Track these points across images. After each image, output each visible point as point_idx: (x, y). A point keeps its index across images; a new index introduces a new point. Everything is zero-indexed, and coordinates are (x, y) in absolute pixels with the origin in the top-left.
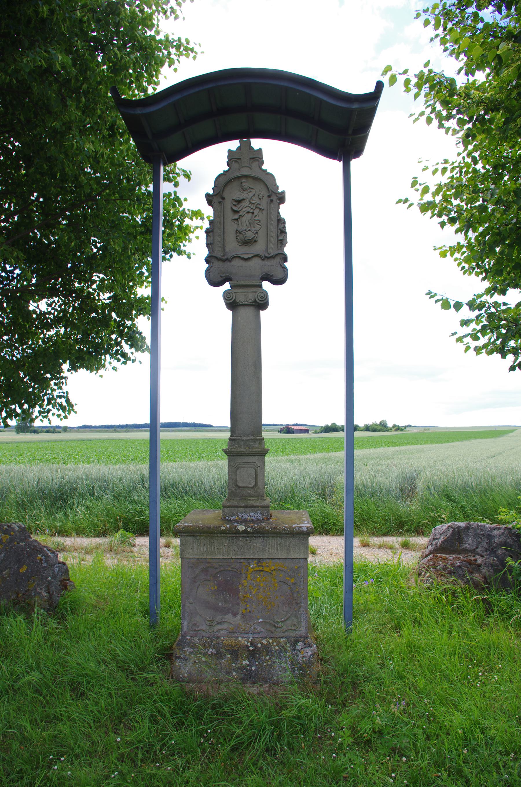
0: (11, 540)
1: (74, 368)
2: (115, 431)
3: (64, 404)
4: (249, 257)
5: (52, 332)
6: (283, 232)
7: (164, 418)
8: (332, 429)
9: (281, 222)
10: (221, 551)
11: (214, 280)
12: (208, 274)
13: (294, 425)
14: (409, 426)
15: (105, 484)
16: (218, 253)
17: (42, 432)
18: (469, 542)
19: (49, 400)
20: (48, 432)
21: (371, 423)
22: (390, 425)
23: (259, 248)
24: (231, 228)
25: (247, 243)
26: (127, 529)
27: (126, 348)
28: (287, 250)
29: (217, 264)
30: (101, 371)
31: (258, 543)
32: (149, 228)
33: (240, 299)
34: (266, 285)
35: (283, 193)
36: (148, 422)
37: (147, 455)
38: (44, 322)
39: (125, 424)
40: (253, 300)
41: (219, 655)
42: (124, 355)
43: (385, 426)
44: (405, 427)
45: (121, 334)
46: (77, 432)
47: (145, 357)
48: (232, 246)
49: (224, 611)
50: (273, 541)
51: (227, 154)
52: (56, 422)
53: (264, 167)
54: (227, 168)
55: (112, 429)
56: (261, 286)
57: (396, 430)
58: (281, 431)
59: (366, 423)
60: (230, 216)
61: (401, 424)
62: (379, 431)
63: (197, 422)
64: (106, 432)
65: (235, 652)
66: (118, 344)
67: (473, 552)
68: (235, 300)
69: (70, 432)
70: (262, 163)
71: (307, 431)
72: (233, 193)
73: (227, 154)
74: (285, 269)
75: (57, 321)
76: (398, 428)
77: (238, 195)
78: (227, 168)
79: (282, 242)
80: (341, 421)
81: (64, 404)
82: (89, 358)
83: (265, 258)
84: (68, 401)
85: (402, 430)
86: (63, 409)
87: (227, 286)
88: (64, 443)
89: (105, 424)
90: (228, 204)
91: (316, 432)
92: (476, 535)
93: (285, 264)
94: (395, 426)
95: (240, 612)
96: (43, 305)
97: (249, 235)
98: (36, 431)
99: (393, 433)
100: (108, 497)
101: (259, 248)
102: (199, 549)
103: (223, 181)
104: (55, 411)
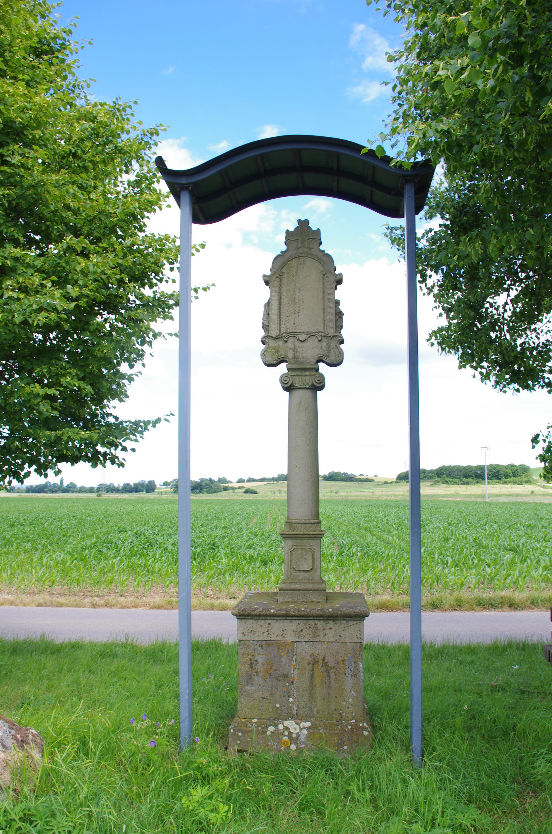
6: (339, 315)
8: (435, 606)
12: (264, 354)
28: (344, 333)
33: (297, 382)
34: (323, 368)
35: (341, 275)
38: (248, 569)
40: (310, 384)
51: (284, 235)
53: (322, 248)
54: (284, 248)
56: (317, 370)
68: (292, 384)
70: (321, 243)
73: (285, 235)
74: (341, 353)
78: (284, 248)
79: (339, 327)
87: (283, 368)
93: (341, 346)
95: (59, 433)
103: (281, 260)
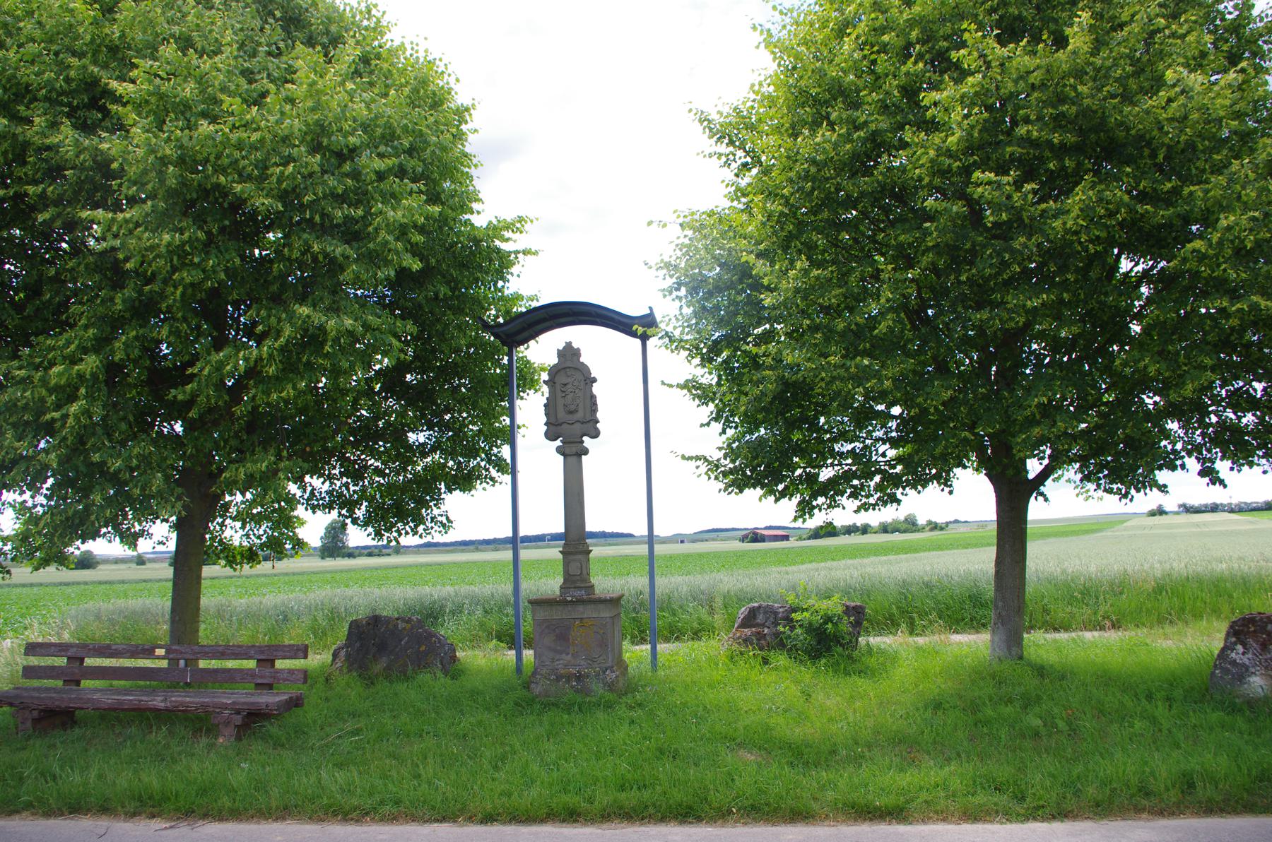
0: (412, 628)
1: (450, 490)
2: (477, 550)
3: (445, 521)
4: (573, 422)
5: (429, 459)
7: (522, 533)
9: (593, 397)
10: (558, 614)
11: (550, 436)
13: (766, 528)
14: (956, 521)
15: (476, 601)
16: (553, 421)
17: (360, 555)
18: (760, 618)
19: (432, 519)
20: (370, 555)
21: (890, 520)
22: (921, 521)
23: (579, 416)
24: (560, 402)
25: (571, 412)
26: (500, 639)
27: (493, 472)
28: (599, 415)
29: (553, 428)
30: (473, 492)
31: (581, 608)
32: (506, 380)
33: (567, 451)
36: (561, 529)
37: (521, 568)
38: (423, 451)
39: (491, 537)
41: (558, 679)
42: (492, 479)
43: (914, 524)
44: (947, 524)
45: (489, 461)
46: (416, 553)
47: (507, 478)
48: (562, 415)
49: (560, 653)
50: (590, 607)
52: (438, 538)
55: (471, 547)
57: (932, 530)
58: (743, 539)
59: (883, 520)
60: (559, 394)
61: (940, 519)
62: (905, 531)
63: (608, 529)
64: (463, 551)
65: (569, 678)
66: (487, 470)
67: (763, 625)
69: (405, 553)
71: (786, 538)
72: (561, 379)
75: (434, 449)
76: (934, 526)
77: (564, 380)
80: (641, 530)
81: (445, 521)
82: (464, 481)
83: (583, 423)
84: (448, 518)
85: (942, 529)
86: (444, 525)
88: (400, 570)
89: (459, 539)
90: (558, 386)
91: (800, 539)
92: (765, 613)
94: (930, 522)
96: (421, 437)
97: (572, 408)
98: (351, 554)
99: (927, 535)
100: (479, 613)
101: (579, 416)
102: (542, 614)
104: (436, 527)
